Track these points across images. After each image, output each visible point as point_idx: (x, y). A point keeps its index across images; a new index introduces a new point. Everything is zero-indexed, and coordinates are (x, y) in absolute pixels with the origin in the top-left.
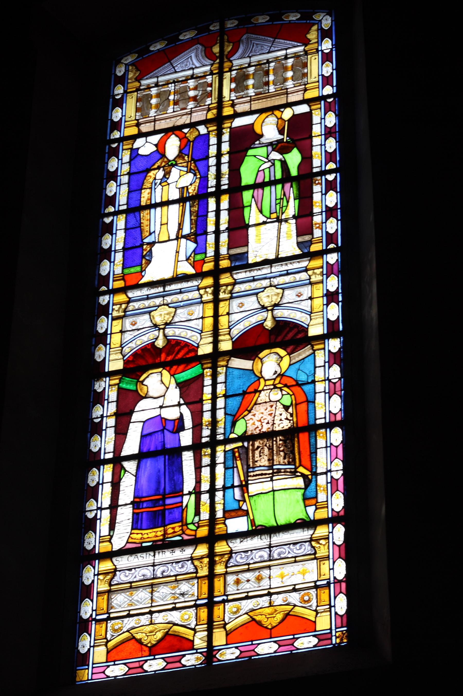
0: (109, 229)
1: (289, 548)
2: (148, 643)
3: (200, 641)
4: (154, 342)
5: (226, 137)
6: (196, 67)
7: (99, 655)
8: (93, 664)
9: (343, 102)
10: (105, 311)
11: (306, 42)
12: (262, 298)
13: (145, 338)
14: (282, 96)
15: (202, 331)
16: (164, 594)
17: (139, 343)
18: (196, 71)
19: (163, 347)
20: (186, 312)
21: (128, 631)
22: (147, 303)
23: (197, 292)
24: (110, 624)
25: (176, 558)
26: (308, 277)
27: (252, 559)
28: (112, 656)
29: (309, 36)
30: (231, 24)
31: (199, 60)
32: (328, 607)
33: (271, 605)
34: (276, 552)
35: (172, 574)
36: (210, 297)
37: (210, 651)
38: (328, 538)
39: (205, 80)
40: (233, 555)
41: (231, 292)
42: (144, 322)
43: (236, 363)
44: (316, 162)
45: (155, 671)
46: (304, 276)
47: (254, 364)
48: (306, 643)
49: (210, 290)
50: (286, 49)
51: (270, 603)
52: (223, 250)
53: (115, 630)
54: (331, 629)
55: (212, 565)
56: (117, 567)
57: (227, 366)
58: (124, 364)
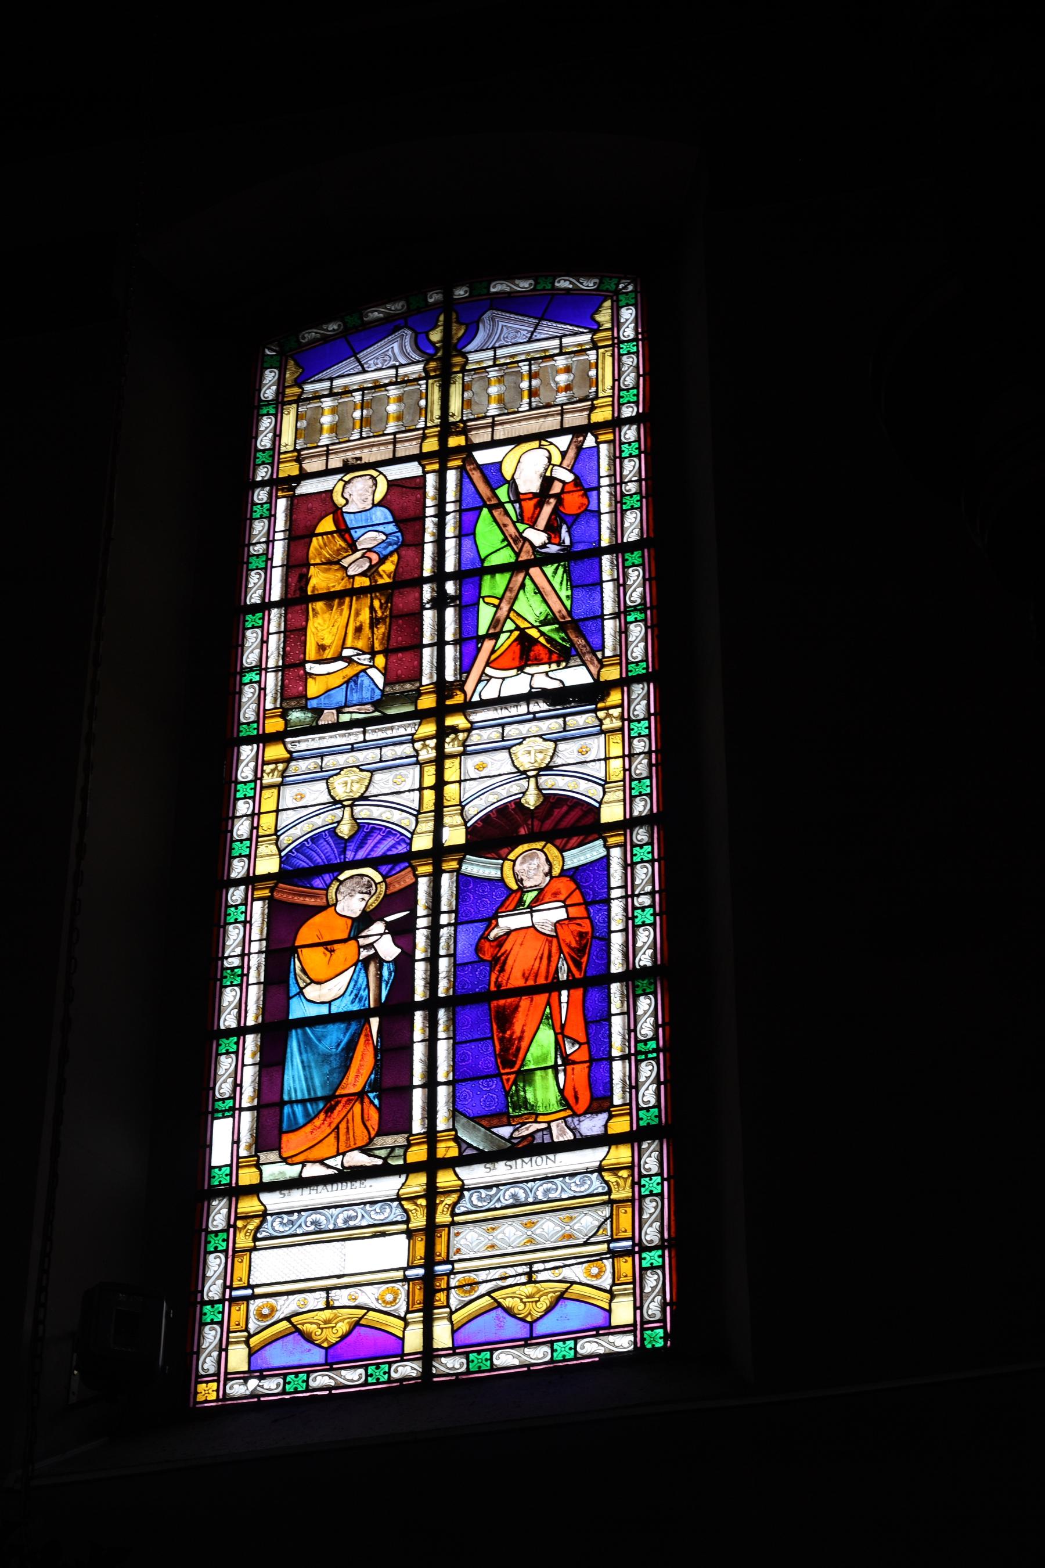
1: (565, 1183)
2: (527, 1316)
4: (335, 828)
6: (402, 365)
11: (595, 328)
12: (335, 785)
15: (419, 812)
18: (402, 371)
19: (537, 808)
20: (391, 778)
21: (288, 1319)
24: (255, 1305)
25: (308, 1203)
27: (499, 1200)
29: (599, 318)
30: (460, 293)
31: (405, 354)
33: (329, 1307)
36: (433, 754)
39: (553, 363)
40: (465, 1193)
43: (477, 867)
49: (432, 743)
51: (328, 1302)
53: (261, 1316)
55: (431, 1211)
58: (281, 862)
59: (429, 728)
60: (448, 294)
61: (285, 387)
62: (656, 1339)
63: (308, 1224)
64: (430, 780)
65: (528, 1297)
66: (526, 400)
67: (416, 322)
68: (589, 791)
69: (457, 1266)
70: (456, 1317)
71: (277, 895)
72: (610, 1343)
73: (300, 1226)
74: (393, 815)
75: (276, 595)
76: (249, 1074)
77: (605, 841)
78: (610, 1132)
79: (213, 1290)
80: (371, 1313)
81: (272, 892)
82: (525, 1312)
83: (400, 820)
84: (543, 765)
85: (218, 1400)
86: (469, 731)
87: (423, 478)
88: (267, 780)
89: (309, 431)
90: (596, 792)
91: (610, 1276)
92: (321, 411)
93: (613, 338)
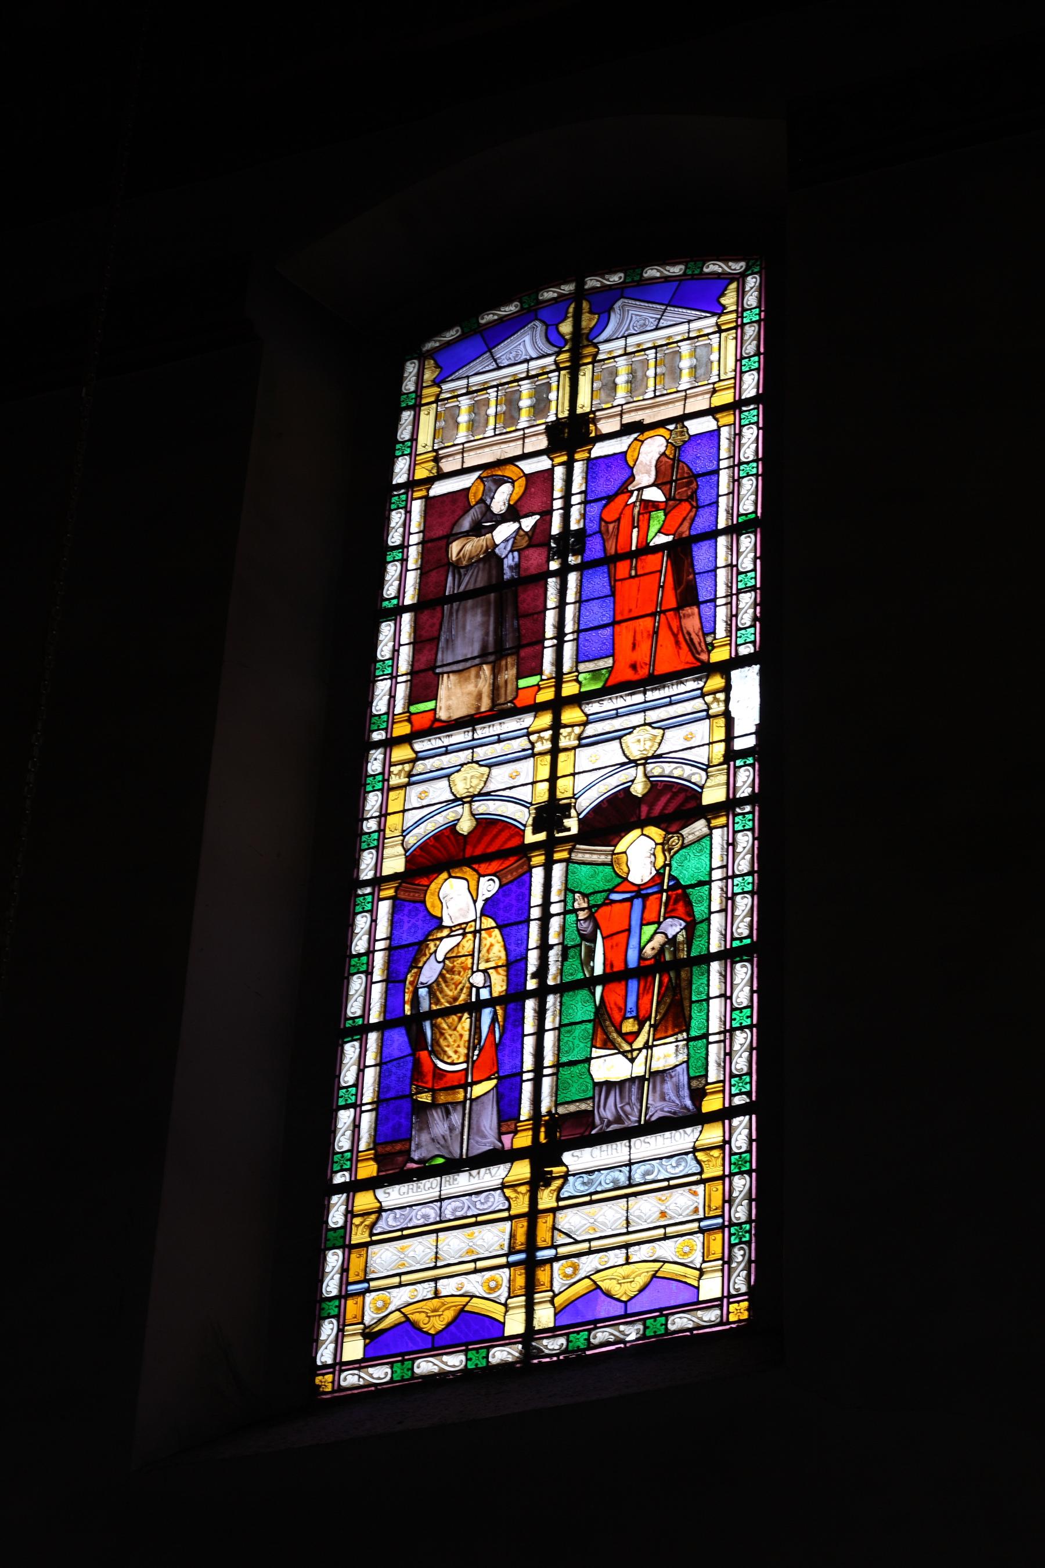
1: (661, 1165)
3: (515, 1325)
6: (532, 359)
12: (457, 782)
19: (644, 795)
23: (700, 700)
27: (600, 1184)
29: (724, 301)
33: (437, 1295)
34: (450, 1208)
36: (548, 745)
41: (410, 775)
42: (439, 792)
49: (548, 734)
50: (689, 322)
56: (383, 1204)
58: (407, 862)
60: (580, 284)
61: (423, 388)
62: (739, 1311)
63: (419, 1217)
64: (544, 772)
65: (624, 1278)
67: (548, 316)
69: (372, 1284)
70: (558, 1301)
71: (402, 895)
72: (443, 1362)
74: (683, 770)
75: (409, 599)
76: (377, 991)
77: (709, 822)
78: (515, 1147)
79: (331, 1286)
81: (570, 854)
82: (622, 1291)
83: (514, 813)
84: (650, 755)
85: (333, 1391)
87: (718, 431)
88: (394, 781)
90: (699, 777)
91: (506, 1289)
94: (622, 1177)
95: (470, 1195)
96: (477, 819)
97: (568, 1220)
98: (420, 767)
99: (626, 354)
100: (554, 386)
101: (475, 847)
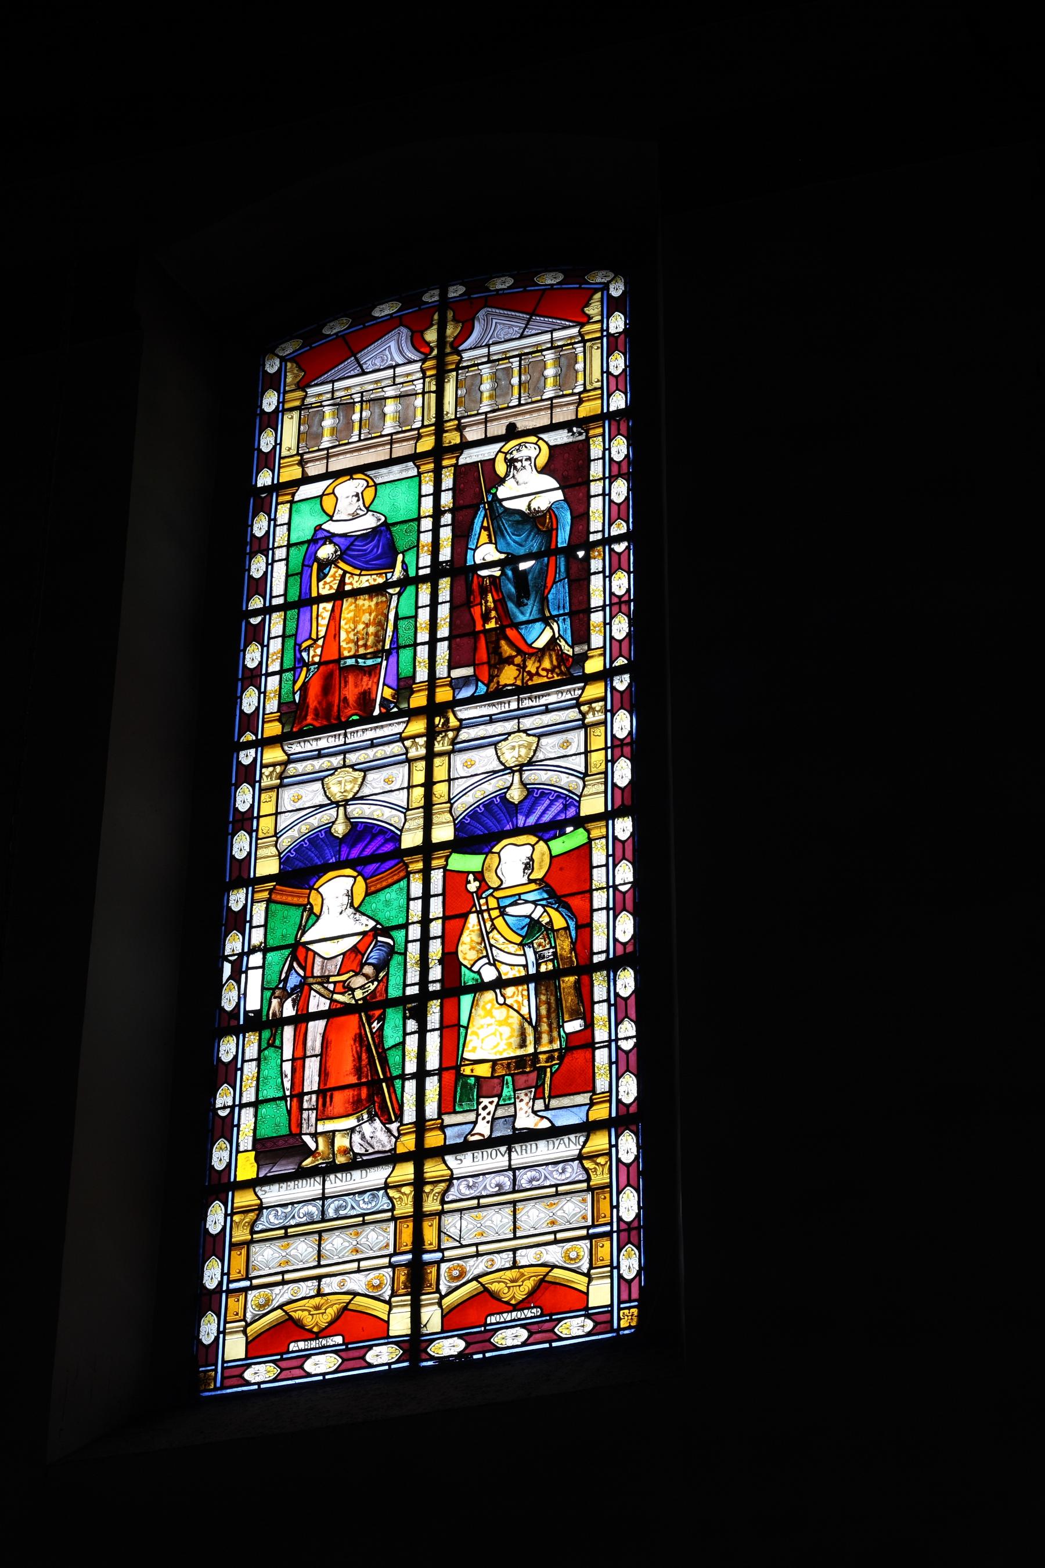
0: (257, 635)
5: (448, 482)
7: (235, 1348)
8: (224, 1362)
9: (631, 422)
10: (249, 775)
12: (330, 785)
13: (314, 821)
14: (542, 413)
15: (586, 774)
16: (534, 1217)
17: (304, 830)
21: (280, 1307)
22: (318, 764)
23: (400, 744)
24: (251, 1294)
26: (404, 751)
27: (485, 1188)
28: (256, 1348)
29: (587, 310)
30: (456, 291)
31: (401, 352)
32: (609, 1269)
35: (547, 1183)
36: (423, 751)
37: (415, 1343)
38: (609, 1154)
40: (455, 1182)
41: (281, 777)
43: (460, 862)
44: (596, 524)
45: (324, 1374)
46: (397, 748)
47: (548, 852)
48: (574, 1328)
49: (422, 741)
52: (442, 670)
54: (611, 1305)
57: (444, 867)
58: (455, 830)
59: (419, 726)
60: (443, 294)
62: (627, 1319)
64: (419, 777)
66: (356, 432)
68: (391, 818)
70: (447, 1302)
73: (293, 1217)
80: (555, 1270)
86: (458, 730)
89: (308, 436)
92: (509, 371)
93: (602, 330)
94: (314, 1210)
95: (547, 1164)
96: (528, 789)
97: (451, 1224)
98: (292, 769)
99: (489, 362)
100: (581, 357)
101: (527, 816)
